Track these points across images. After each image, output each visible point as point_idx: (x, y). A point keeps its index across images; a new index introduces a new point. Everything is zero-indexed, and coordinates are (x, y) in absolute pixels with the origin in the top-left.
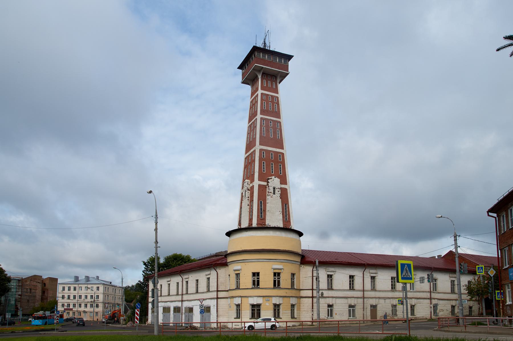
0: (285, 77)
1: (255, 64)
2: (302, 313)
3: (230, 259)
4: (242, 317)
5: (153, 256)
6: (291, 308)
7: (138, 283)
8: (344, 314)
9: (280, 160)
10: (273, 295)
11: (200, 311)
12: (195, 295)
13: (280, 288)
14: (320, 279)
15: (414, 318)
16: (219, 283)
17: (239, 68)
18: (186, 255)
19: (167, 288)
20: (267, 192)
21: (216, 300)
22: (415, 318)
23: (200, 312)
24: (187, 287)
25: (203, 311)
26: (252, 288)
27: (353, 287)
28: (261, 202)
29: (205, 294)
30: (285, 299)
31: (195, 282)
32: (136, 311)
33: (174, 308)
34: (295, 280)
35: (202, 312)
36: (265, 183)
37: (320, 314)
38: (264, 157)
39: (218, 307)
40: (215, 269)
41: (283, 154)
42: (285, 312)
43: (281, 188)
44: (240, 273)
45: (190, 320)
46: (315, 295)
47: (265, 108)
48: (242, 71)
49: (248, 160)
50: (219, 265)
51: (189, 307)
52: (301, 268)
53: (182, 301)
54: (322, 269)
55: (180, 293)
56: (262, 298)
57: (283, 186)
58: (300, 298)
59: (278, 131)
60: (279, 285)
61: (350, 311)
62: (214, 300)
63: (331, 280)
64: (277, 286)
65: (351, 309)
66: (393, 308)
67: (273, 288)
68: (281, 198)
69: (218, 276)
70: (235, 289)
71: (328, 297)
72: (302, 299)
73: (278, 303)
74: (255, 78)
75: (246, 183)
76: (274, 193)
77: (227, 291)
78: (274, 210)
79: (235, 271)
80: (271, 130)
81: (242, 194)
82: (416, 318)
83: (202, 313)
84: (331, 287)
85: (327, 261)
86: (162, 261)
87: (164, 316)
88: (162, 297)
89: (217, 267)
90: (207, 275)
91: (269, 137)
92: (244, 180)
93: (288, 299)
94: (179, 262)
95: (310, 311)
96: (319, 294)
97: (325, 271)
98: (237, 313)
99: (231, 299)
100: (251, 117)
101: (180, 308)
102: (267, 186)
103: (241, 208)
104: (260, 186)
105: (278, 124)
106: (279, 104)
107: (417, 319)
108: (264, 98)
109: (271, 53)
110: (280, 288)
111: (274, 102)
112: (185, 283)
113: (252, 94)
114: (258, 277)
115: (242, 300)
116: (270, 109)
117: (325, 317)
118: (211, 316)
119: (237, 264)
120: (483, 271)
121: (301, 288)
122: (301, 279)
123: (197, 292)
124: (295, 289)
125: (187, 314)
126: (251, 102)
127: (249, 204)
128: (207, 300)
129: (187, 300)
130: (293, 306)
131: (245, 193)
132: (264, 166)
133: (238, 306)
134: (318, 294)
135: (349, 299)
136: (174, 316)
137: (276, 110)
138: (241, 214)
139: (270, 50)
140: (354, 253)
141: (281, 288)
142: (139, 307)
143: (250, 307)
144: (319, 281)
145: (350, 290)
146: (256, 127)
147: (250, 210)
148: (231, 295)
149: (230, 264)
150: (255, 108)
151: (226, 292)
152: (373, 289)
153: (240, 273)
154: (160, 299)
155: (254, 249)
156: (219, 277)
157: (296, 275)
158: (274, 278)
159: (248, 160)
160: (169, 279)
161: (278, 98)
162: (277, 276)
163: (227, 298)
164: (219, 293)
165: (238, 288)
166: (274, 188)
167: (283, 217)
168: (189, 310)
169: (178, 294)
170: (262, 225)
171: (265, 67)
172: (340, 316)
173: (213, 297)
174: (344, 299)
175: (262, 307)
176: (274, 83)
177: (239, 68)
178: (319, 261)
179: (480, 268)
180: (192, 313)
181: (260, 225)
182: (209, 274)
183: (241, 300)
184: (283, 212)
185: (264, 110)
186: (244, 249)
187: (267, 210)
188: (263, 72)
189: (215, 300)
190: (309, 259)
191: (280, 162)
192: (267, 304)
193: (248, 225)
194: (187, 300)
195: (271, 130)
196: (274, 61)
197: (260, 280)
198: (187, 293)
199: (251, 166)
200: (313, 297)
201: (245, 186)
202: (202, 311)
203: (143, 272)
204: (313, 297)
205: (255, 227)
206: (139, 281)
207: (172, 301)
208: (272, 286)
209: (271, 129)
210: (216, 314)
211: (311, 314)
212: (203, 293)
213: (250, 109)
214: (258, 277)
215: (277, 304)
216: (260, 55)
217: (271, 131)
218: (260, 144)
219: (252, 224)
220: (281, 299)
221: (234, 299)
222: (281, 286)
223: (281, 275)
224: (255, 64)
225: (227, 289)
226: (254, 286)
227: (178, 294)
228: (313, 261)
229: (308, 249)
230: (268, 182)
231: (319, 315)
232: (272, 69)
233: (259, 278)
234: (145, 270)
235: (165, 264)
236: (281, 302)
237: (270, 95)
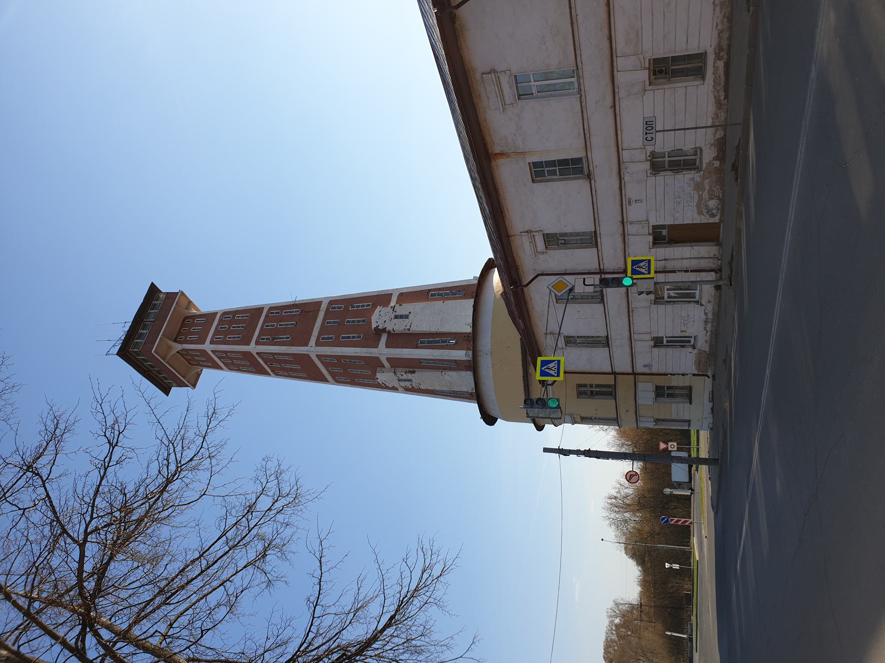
15: (721, 64)
22: (718, 57)
32: (672, 523)
66: (663, 396)
82: (719, 48)
107: (725, 43)
120: (552, 361)
142: (666, 519)
152: (592, 240)
179: (543, 368)
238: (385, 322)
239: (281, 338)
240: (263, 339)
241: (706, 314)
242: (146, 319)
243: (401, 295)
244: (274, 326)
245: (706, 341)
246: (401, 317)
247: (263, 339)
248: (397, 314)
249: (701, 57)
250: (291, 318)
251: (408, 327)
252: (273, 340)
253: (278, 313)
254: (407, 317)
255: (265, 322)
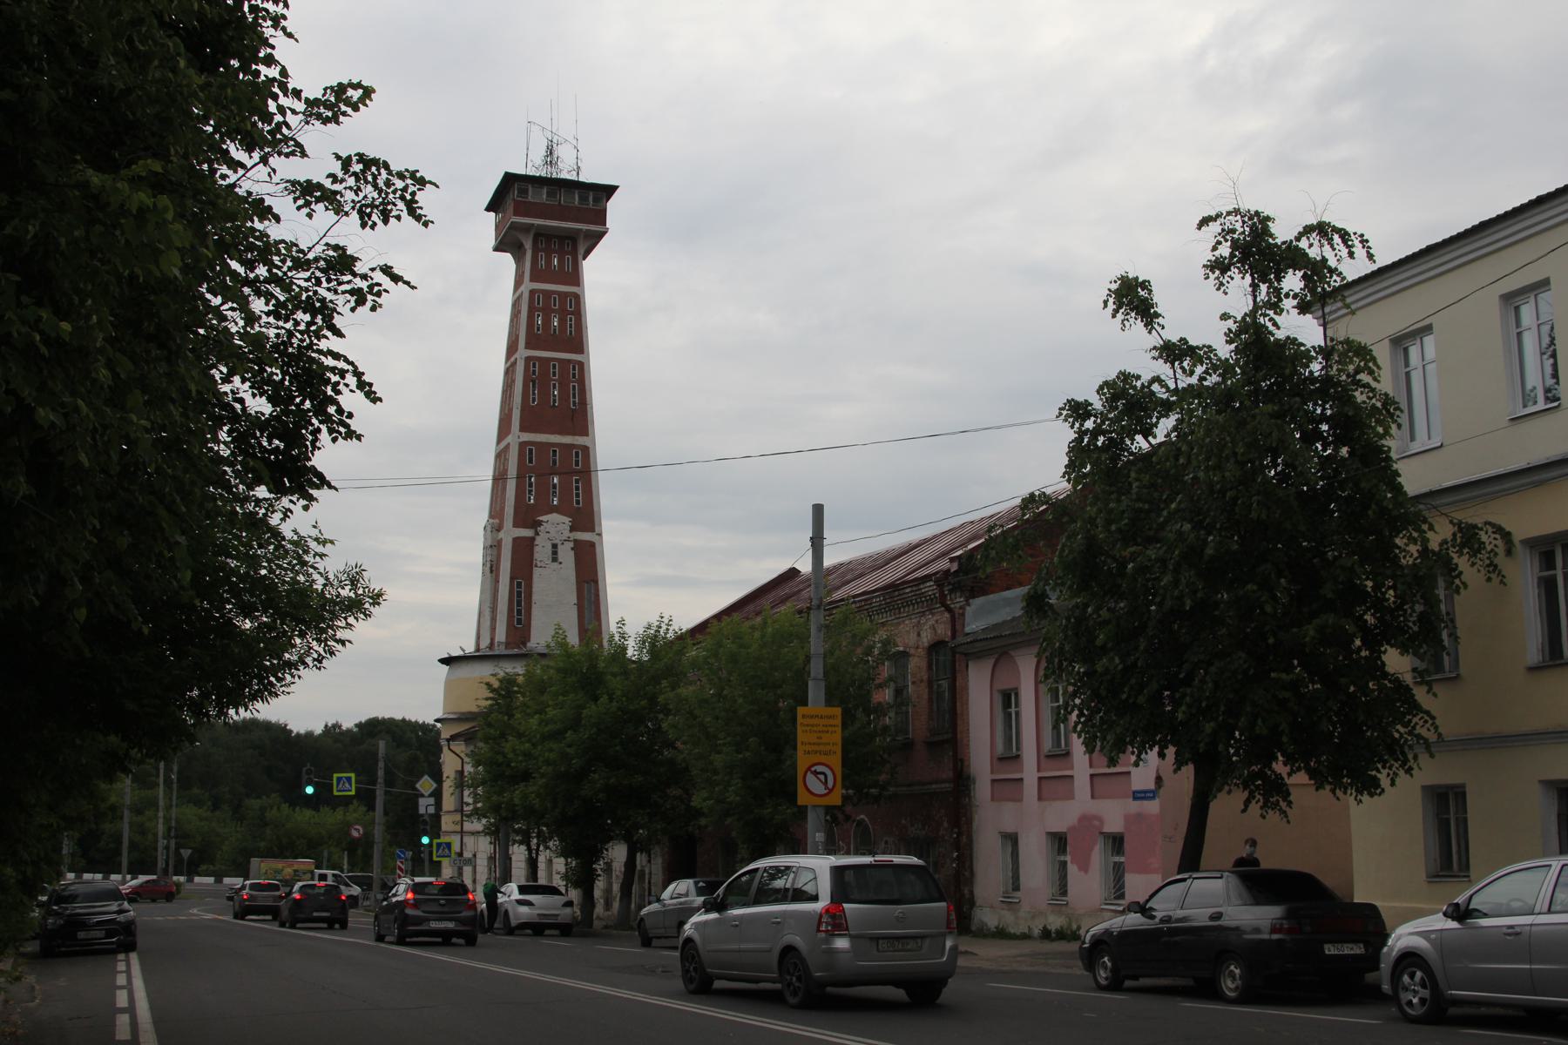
17: (488, 209)
32: (398, 863)
120: (351, 785)
188: (1554, 843)
238: (548, 532)
239: (534, 391)
240: (534, 366)
243: (592, 545)
244: (554, 375)
246: (555, 553)
247: (534, 366)
248: (560, 547)
249: (537, 881)
250: (564, 396)
251: (539, 564)
252: (532, 381)
253: (574, 377)
254: (555, 560)
255: (560, 361)
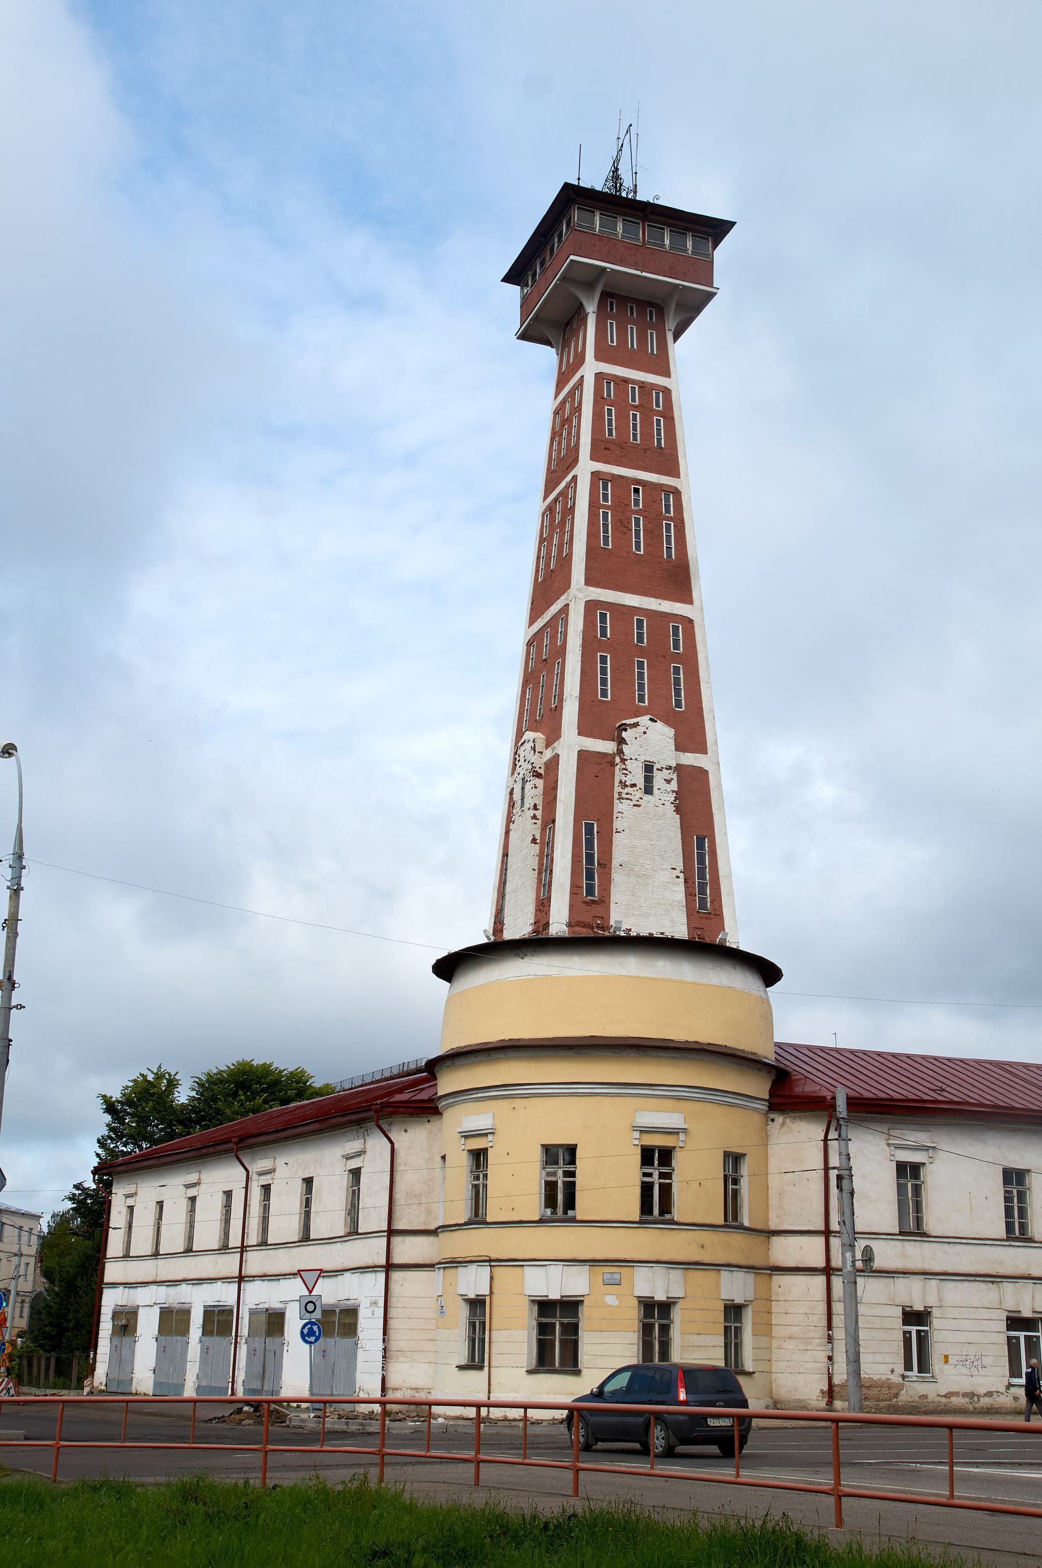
0: (698, 309)
1: (572, 257)
2: (779, 1348)
3: (448, 1083)
4: (493, 1364)
5: (146, 1072)
6: (726, 1320)
7: (74, 1195)
8: (986, 1361)
9: (676, 647)
10: (635, 1257)
11: (304, 1327)
12: (294, 1249)
13: (672, 1222)
14: (857, 1183)
16: (399, 1196)
17: (507, 279)
18: (291, 1070)
19: (182, 1217)
20: (617, 783)
21: (382, 1276)
23: (302, 1333)
24: (264, 1213)
25: (315, 1328)
26: (542, 1221)
27: (1023, 1227)
28: (589, 828)
29: (339, 1244)
30: (698, 1276)
31: (299, 1187)
33: (205, 1312)
34: (744, 1184)
35: (311, 1333)
36: (607, 747)
37: (863, 1358)
38: (604, 633)
39: (392, 1313)
40: (385, 1128)
41: (691, 621)
42: (696, 1340)
43: (679, 769)
44: (486, 1149)
45: (267, 1375)
46: (836, 1262)
47: (610, 434)
48: (522, 289)
49: (539, 652)
50: (401, 1110)
51: (267, 1310)
52: (774, 1128)
53: (241, 1279)
54: (870, 1137)
55: (235, 1241)
56: (586, 1268)
57: (689, 759)
58: (770, 1275)
59: (668, 526)
60: (666, 1206)
61: (1012, 1345)
62: (373, 1274)
63: (917, 1190)
64: (656, 1211)
65: (1022, 1335)
67: (641, 1222)
68: (678, 810)
69: (398, 1161)
70: (466, 1224)
71: (905, 1273)
72: (779, 1280)
73: (660, 1297)
74: (573, 316)
75: (528, 746)
76: (648, 790)
77: (434, 1233)
78: (648, 862)
79: (466, 1137)
80: (637, 524)
81: (511, 793)
83: (312, 1339)
84: (919, 1221)
85: (892, 1100)
86: (183, 1095)
87: (162, 1351)
88: (161, 1262)
89: (395, 1118)
90: (348, 1157)
91: (630, 552)
92: (520, 734)
93: (711, 1275)
94: (259, 1101)
95: (817, 1341)
96: (854, 1257)
97: (884, 1142)
98: (472, 1341)
99: (448, 1271)
100: (554, 472)
101: (232, 1311)
102: (618, 760)
103: (505, 855)
104: (584, 756)
105: (667, 500)
106: (673, 418)
108: (609, 395)
109: (640, 214)
110: (672, 1222)
111: (652, 410)
112: (256, 1193)
113: (562, 380)
114: (570, 1168)
115: (495, 1276)
116: (635, 439)
117: (892, 1371)
118: (360, 1352)
119: (479, 1104)
121: (773, 1226)
122: (774, 1181)
123: (306, 1238)
124: (742, 1228)
125: (258, 1343)
126: (556, 413)
127: (538, 837)
128: (347, 1275)
129: (263, 1277)
130: (733, 1311)
131: (523, 789)
132: (604, 671)
133: (477, 1305)
134: (848, 1255)
135: (1008, 1287)
136: (205, 1351)
137: (659, 440)
138: (505, 883)
139: (578, 187)
140: (1026, 1066)
141: (677, 1223)
143: (531, 1310)
144: (852, 1193)
145: (1008, 1239)
146: (572, 510)
147: (541, 864)
148: (449, 1254)
149: (451, 1105)
150: (569, 433)
151: (431, 1239)
153: (486, 1149)
154: (112, 1272)
155: (551, 1036)
156: (399, 1168)
157: (747, 1157)
158: (645, 1175)
159: (539, 652)
160: (192, 1178)
161: (667, 392)
162: (656, 1162)
163: (431, 1266)
164: (396, 1240)
165: (478, 1219)
166: (649, 768)
167: (689, 894)
168: (269, 1323)
169: (224, 1248)
170: (593, 928)
171: (612, 270)
172: (965, 1371)
173: (370, 1263)
174: (982, 1285)
175: (586, 1315)
176: (652, 335)
177: (507, 279)
178: (848, 1098)
180: (350, 1341)
181: (584, 930)
182: (359, 1154)
183: (492, 1278)
184: (687, 871)
185: (608, 441)
186: (507, 1036)
187: (615, 863)
189: (378, 1274)
190: (809, 1088)
191: (677, 657)
192: (611, 1300)
193: (530, 928)
194: (263, 1277)
195: (637, 524)
196: (654, 244)
197: (579, 1180)
198: (264, 1243)
199: (551, 672)
200: (828, 1271)
201: (522, 760)
202: (311, 1329)
203: (102, 1143)
204: (828, 1271)
205: (560, 934)
206: (76, 1187)
207: (199, 1281)
208: (632, 1209)
209: (637, 520)
210: (381, 1346)
211: (822, 1356)
212: (330, 1240)
213: (552, 439)
214: (570, 1168)
215: (656, 1298)
216: (593, 222)
217: (639, 526)
218: (590, 581)
219: (547, 925)
220: (676, 1275)
221: (461, 1270)
222: (677, 1214)
223: (679, 1161)
224: (572, 257)
225: (432, 1227)
226: (549, 1211)
227: (224, 1248)
228: (825, 1097)
229: (831, 1044)
230: (622, 741)
231: (854, 1360)
232: (644, 274)
233: (572, 1174)
234: (110, 1137)
235: (194, 1109)
236: (676, 1292)
237: (634, 382)
241: (989, 1394)
242: (648, 225)
245: (925, 1396)
